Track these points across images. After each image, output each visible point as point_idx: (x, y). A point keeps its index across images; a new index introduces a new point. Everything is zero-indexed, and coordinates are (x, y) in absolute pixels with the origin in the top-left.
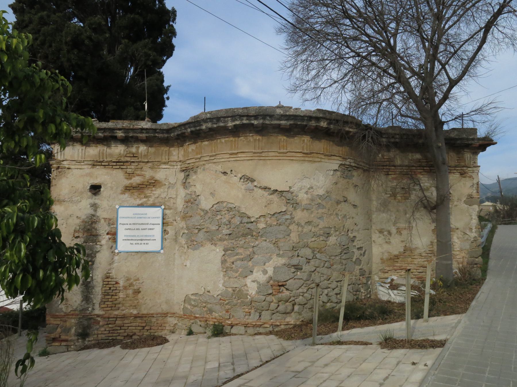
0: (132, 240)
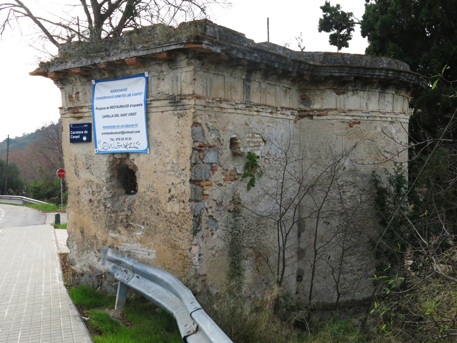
0: (112, 133)
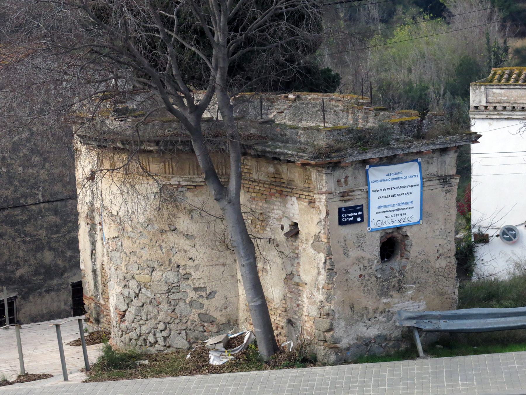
0: (387, 211)
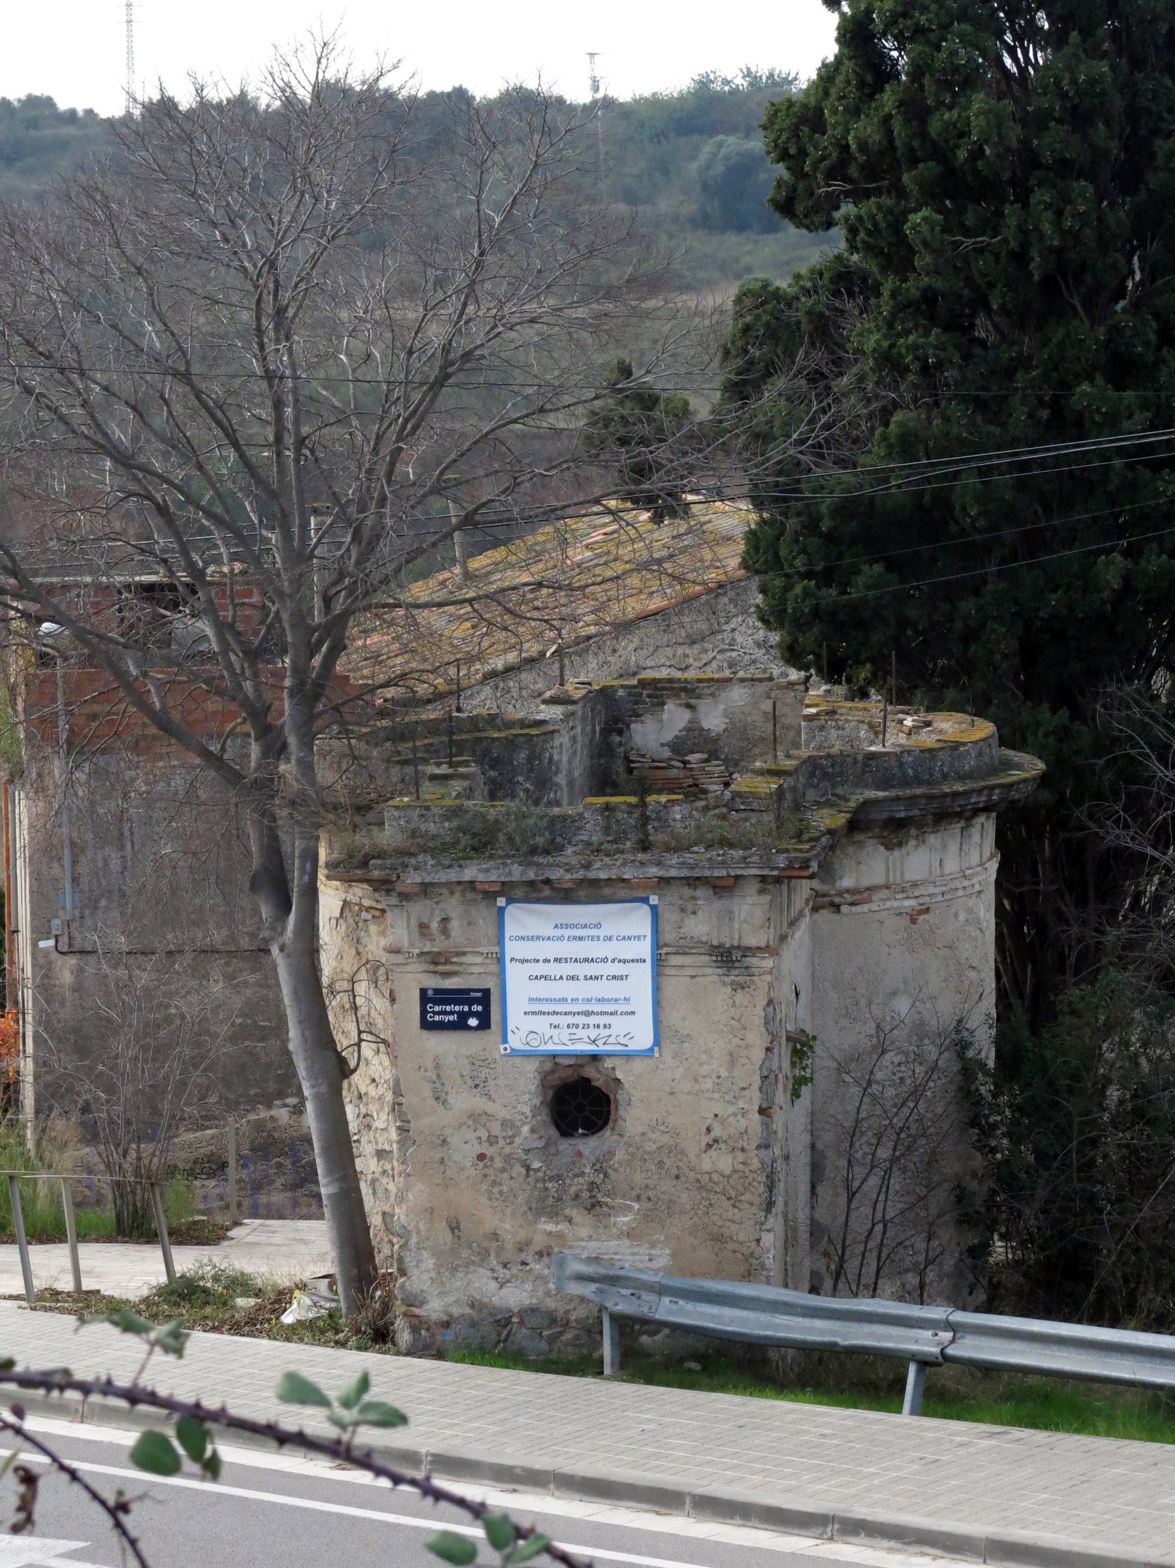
0: (555, 1013)
